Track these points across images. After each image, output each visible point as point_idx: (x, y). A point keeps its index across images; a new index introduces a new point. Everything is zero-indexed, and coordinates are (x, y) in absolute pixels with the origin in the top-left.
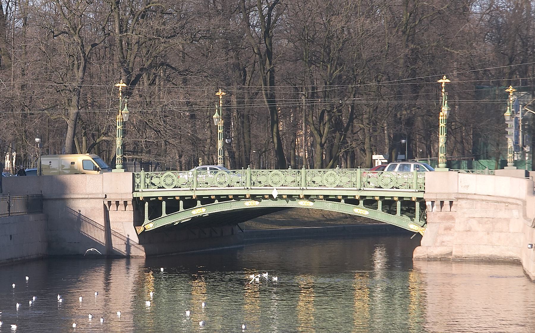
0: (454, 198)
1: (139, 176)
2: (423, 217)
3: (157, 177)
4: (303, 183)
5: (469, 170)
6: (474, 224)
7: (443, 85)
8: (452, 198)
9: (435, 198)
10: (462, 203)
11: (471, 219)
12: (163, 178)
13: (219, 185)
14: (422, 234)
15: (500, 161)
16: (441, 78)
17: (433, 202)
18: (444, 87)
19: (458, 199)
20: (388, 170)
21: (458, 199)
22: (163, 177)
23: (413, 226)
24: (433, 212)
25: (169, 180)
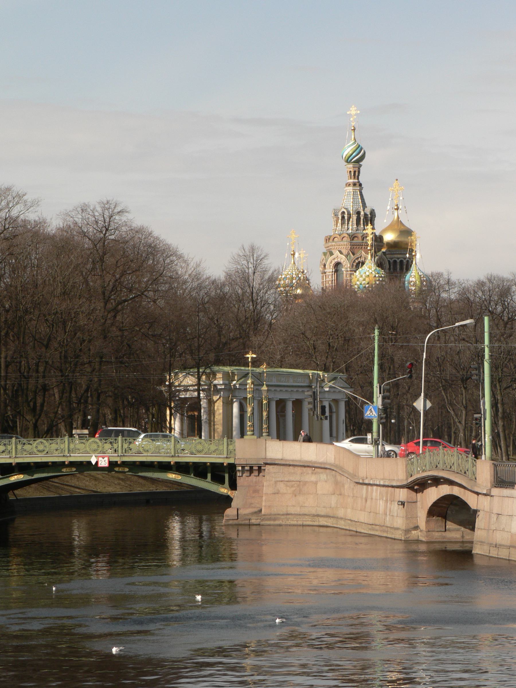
0: (262, 463)
1: (10, 443)
2: (233, 486)
3: (29, 444)
4: (120, 451)
5: (102, 438)
6: (281, 487)
7: (250, 360)
8: (260, 463)
9: (245, 463)
10: (268, 467)
11: (278, 483)
12: (35, 445)
13: (38, 453)
14: (232, 497)
15: (370, 423)
16: (248, 353)
17: (243, 467)
18: (251, 361)
19: (266, 464)
20: (350, 441)
21: (266, 464)
22: (35, 444)
23: (224, 490)
24: (242, 481)
25: (41, 447)
